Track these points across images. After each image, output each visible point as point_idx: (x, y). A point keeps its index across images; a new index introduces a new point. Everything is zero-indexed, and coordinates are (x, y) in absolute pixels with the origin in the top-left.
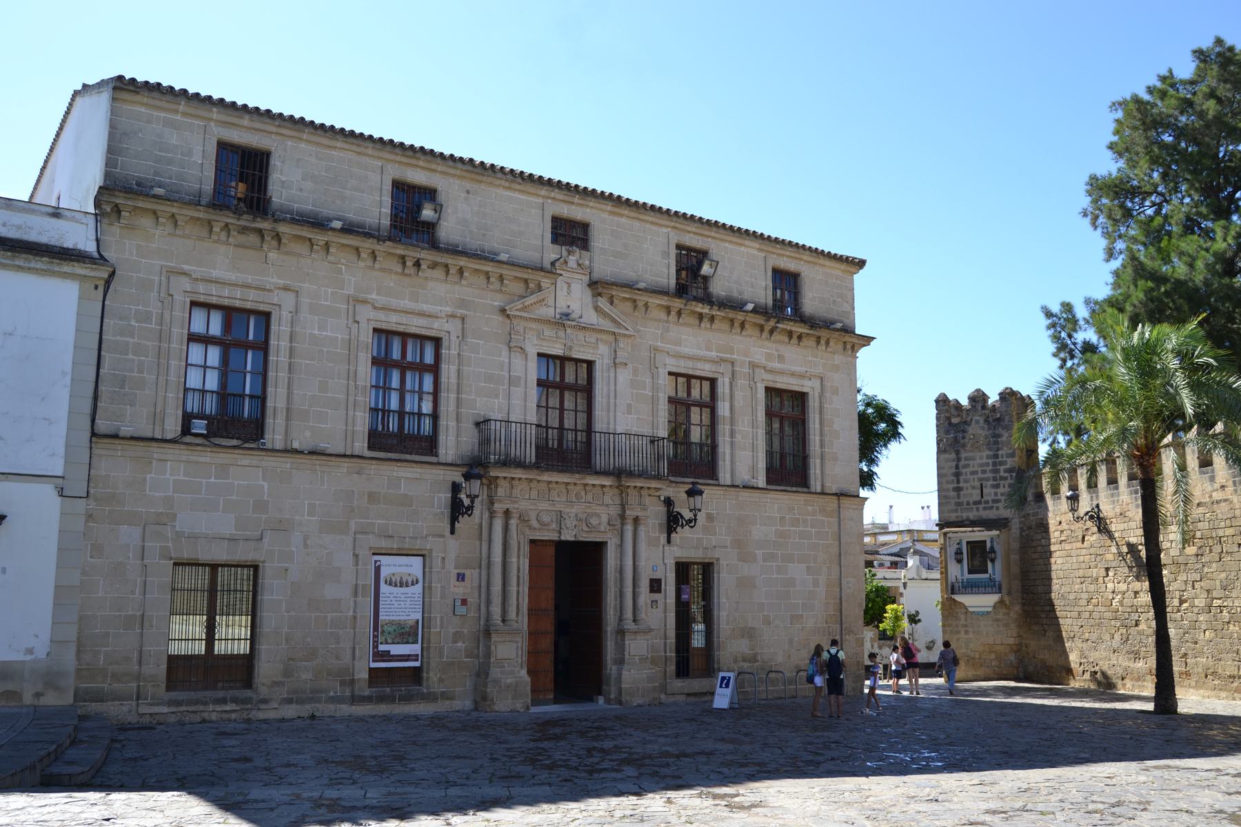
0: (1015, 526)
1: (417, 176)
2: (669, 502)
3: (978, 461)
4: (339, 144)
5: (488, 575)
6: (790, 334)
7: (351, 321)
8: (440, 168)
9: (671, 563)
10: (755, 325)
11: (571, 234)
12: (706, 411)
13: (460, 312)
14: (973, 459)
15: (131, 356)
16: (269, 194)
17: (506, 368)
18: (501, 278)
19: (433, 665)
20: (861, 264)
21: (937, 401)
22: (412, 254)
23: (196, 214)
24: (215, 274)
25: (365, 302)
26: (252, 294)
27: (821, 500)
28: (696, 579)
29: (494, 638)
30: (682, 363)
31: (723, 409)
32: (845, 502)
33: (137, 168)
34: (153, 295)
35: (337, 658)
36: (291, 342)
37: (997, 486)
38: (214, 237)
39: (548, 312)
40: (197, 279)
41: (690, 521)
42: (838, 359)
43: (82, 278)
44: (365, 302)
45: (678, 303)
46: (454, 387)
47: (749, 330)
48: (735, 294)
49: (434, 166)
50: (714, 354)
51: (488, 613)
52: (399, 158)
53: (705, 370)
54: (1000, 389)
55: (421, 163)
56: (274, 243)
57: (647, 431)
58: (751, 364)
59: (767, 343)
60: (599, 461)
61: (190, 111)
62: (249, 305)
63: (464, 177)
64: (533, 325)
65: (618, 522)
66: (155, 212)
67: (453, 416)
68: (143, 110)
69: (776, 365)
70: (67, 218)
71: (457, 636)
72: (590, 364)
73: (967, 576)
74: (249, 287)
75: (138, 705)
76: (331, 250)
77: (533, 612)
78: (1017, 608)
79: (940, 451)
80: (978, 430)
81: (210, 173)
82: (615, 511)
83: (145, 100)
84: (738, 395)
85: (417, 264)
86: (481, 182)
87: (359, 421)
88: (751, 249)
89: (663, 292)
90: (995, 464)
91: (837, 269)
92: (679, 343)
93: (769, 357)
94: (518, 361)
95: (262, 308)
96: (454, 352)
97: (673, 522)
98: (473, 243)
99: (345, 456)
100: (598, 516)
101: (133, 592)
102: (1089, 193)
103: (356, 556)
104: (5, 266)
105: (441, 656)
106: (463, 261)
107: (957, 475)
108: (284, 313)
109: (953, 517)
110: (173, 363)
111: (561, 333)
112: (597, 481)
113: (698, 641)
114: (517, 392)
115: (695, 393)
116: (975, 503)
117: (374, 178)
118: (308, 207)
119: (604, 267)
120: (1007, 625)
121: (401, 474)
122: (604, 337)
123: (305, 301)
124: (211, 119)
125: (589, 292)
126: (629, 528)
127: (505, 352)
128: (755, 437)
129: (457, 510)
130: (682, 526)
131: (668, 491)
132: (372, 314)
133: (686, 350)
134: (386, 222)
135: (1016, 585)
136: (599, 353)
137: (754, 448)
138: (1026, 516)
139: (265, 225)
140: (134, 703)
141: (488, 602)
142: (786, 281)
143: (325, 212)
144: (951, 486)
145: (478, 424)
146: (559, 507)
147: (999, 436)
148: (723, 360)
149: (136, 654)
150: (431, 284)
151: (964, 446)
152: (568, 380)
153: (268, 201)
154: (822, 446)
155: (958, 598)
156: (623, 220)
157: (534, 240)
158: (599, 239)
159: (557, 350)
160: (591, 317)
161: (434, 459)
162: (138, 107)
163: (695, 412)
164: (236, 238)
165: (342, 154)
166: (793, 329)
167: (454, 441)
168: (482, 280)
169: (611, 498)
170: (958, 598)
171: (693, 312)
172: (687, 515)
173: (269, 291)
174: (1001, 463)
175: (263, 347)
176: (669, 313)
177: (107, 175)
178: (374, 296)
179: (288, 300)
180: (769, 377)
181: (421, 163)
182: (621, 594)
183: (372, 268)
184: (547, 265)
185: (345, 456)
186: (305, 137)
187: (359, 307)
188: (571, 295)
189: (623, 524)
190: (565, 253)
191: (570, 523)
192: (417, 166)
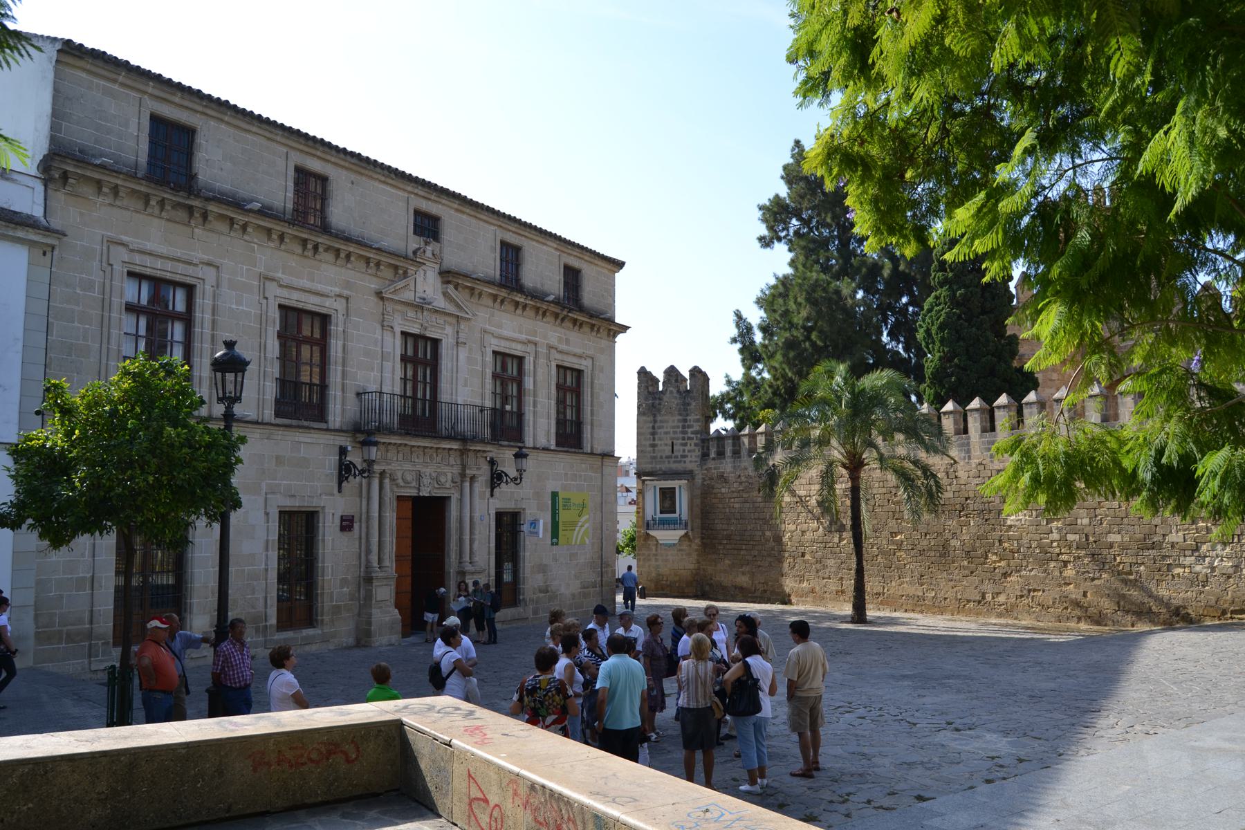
0: (698, 480)
1: (315, 165)
2: (492, 462)
3: (671, 424)
4: (254, 129)
5: (368, 528)
6: (575, 321)
7: (104, 264)
8: (333, 159)
9: (493, 512)
10: (491, 294)
11: (427, 226)
12: (316, 349)
13: (346, 292)
14: (667, 422)
15: (76, 324)
16: (194, 171)
17: (379, 344)
18: (378, 264)
19: (326, 609)
20: (620, 265)
21: (639, 373)
22: (108, 179)
23: (137, 188)
24: (149, 246)
25: (273, 280)
26: (181, 268)
27: (591, 460)
28: (509, 527)
29: (375, 583)
30: (503, 343)
31: (336, 347)
32: (607, 461)
33: (80, 135)
34: (96, 264)
35: (253, 607)
36: (213, 315)
37: (685, 445)
38: (149, 210)
39: (408, 296)
40: (133, 251)
41: (516, 479)
42: (604, 343)
43: (32, 244)
44: (273, 280)
45: (503, 293)
46: (340, 361)
47: (549, 318)
48: (539, 286)
49: (328, 157)
50: (523, 337)
51: (368, 561)
52: (301, 147)
53: (517, 349)
54: (690, 367)
55: (318, 153)
56: (200, 220)
57: (478, 402)
58: (544, 342)
59: (559, 329)
60: (444, 425)
61: (129, 82)
62: (178, 278)
63: (351, 170)
64: (399, 307)
65: (458, 479)
66: (232, 219)
67: (339, 387)
68: (84, 75)
69: (564, 347)
70: (13, 181)
71: (344, 582)
72: (436, 342)
73: (659, 515)
74: (178, 260)
75: (90, 663)
76: (249, 229)
77: (399, 558)
78: (698, 541)
79: (640, 414)
80: (672, 401)
81: (144, 146)
82: (456, 470)
83: (88, 67)
84: (540, 371)
85: (316, 248)
86: (362, 174)
87: (268, 391)
88: (549, 249)
89: (490, 283)
90: (684, 427)
91: (604, 267)
92: (500, 327)
93: (560, 340)
94: (388, 337)
95: (189, 281)
96: (340, 329)
97: (496, 478)
98: (355, 230)
99: (257, 423)
100: (445, 474)
101: (83, 555)
102: (764, 220)
103: (267, 514)
104: (5, 237)
105: (332, 601)
106: (352, 248)
107: (653, 434)
108: (208, 287)
109: (648, 467)
110: (205, 345)
111: (419, 314)
112: (446, 445)
113: (507, 577)
114: (388, 365)
115: (306, 332)
116: (667, 457)
117: (281, 163)
118: (227, 187)
119: (454, 258)
120: (689, 555)
121: (301, 439)
122: (450, 319)
123: (225, 276)
124: (145, 93)
125: (439, 280)
126: (467, 484)
127: (379, 331)
128: (549, 404)
129: (345, 471)
130: (355, 476)
131: (493, 451)
132: (279, 292)
133: (506, 333)
134: (143, 159)
135: (698, 522)
136: (445, 334)
137: (549, 417)
138: (708, 470)
139: (196, 203)
140: (86, 661)
141: (368, 552)
142: (572, 277)
143: (243, 192)
144: (648, 443)
145: (358, 394)
146: (419, 468)
147: (689, 404)
148: (530, 342)
149: (87, 615)
150: (324, 266)
151: (659, 411)
152: (422, 356)
153: (192, 177)
154: (592, 414)
155: (652, 533)
156: (464, 217)
157: (396, 230)
158: (449, 232)
159: (415, 330)
160: (440, 303)
161: (323, 426)
162: (78, 74)
163: (305, 351)
164: (169, 212)
165: (254, 139)
166: (342, 247)
167: (340, 409)
168: (362, 265)
169: (454, 460)
170: (652, 533)
171: (513, 300)
172: (513, 473)
173: (195, 265)
174: (689, 427)
175: (188, 319)
176: (495, 301)
177: (53, 139)
178: (280, 275)
179: (210, 274)
180: (559, 356)
181: (279, 138)
182: (461, 541)
183: (278, 249)
184: (410, 254)
185: (257, 423)
186: (226, 118)
187: (268, 283)
188: (427, 284)
189: (462, 481)
190: (422, 244)
191: (426, 481)
192: (314, 155)
